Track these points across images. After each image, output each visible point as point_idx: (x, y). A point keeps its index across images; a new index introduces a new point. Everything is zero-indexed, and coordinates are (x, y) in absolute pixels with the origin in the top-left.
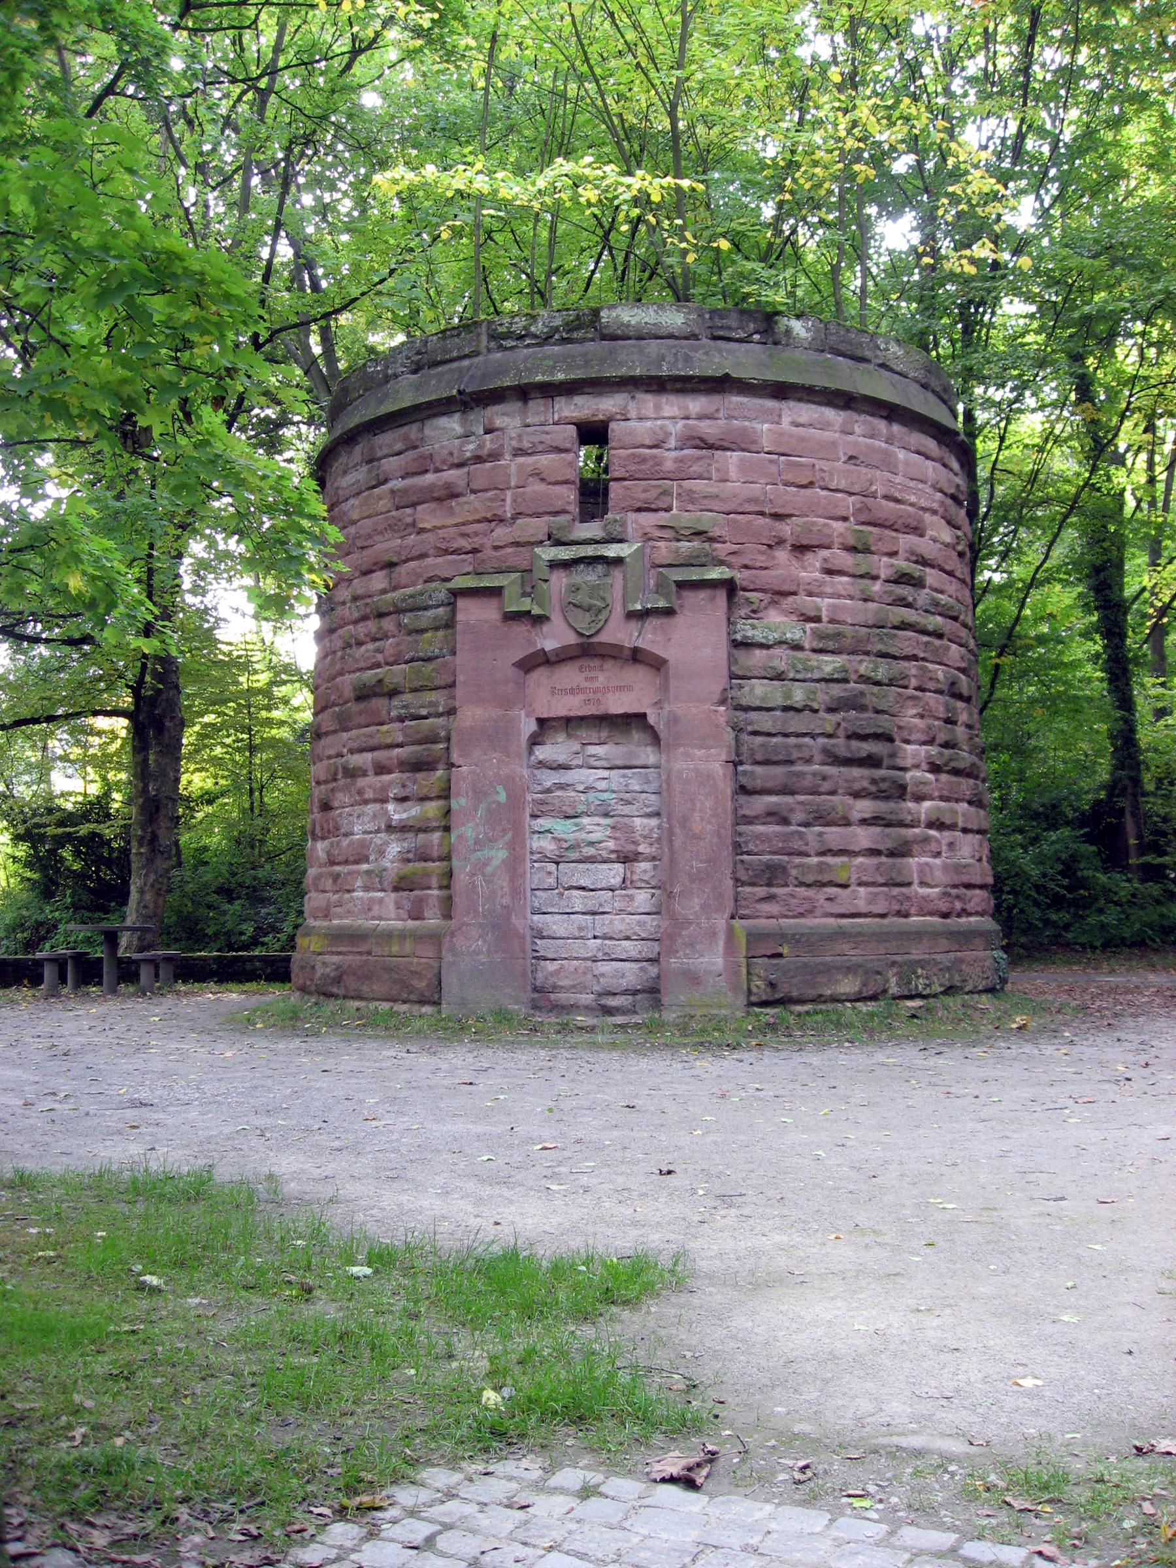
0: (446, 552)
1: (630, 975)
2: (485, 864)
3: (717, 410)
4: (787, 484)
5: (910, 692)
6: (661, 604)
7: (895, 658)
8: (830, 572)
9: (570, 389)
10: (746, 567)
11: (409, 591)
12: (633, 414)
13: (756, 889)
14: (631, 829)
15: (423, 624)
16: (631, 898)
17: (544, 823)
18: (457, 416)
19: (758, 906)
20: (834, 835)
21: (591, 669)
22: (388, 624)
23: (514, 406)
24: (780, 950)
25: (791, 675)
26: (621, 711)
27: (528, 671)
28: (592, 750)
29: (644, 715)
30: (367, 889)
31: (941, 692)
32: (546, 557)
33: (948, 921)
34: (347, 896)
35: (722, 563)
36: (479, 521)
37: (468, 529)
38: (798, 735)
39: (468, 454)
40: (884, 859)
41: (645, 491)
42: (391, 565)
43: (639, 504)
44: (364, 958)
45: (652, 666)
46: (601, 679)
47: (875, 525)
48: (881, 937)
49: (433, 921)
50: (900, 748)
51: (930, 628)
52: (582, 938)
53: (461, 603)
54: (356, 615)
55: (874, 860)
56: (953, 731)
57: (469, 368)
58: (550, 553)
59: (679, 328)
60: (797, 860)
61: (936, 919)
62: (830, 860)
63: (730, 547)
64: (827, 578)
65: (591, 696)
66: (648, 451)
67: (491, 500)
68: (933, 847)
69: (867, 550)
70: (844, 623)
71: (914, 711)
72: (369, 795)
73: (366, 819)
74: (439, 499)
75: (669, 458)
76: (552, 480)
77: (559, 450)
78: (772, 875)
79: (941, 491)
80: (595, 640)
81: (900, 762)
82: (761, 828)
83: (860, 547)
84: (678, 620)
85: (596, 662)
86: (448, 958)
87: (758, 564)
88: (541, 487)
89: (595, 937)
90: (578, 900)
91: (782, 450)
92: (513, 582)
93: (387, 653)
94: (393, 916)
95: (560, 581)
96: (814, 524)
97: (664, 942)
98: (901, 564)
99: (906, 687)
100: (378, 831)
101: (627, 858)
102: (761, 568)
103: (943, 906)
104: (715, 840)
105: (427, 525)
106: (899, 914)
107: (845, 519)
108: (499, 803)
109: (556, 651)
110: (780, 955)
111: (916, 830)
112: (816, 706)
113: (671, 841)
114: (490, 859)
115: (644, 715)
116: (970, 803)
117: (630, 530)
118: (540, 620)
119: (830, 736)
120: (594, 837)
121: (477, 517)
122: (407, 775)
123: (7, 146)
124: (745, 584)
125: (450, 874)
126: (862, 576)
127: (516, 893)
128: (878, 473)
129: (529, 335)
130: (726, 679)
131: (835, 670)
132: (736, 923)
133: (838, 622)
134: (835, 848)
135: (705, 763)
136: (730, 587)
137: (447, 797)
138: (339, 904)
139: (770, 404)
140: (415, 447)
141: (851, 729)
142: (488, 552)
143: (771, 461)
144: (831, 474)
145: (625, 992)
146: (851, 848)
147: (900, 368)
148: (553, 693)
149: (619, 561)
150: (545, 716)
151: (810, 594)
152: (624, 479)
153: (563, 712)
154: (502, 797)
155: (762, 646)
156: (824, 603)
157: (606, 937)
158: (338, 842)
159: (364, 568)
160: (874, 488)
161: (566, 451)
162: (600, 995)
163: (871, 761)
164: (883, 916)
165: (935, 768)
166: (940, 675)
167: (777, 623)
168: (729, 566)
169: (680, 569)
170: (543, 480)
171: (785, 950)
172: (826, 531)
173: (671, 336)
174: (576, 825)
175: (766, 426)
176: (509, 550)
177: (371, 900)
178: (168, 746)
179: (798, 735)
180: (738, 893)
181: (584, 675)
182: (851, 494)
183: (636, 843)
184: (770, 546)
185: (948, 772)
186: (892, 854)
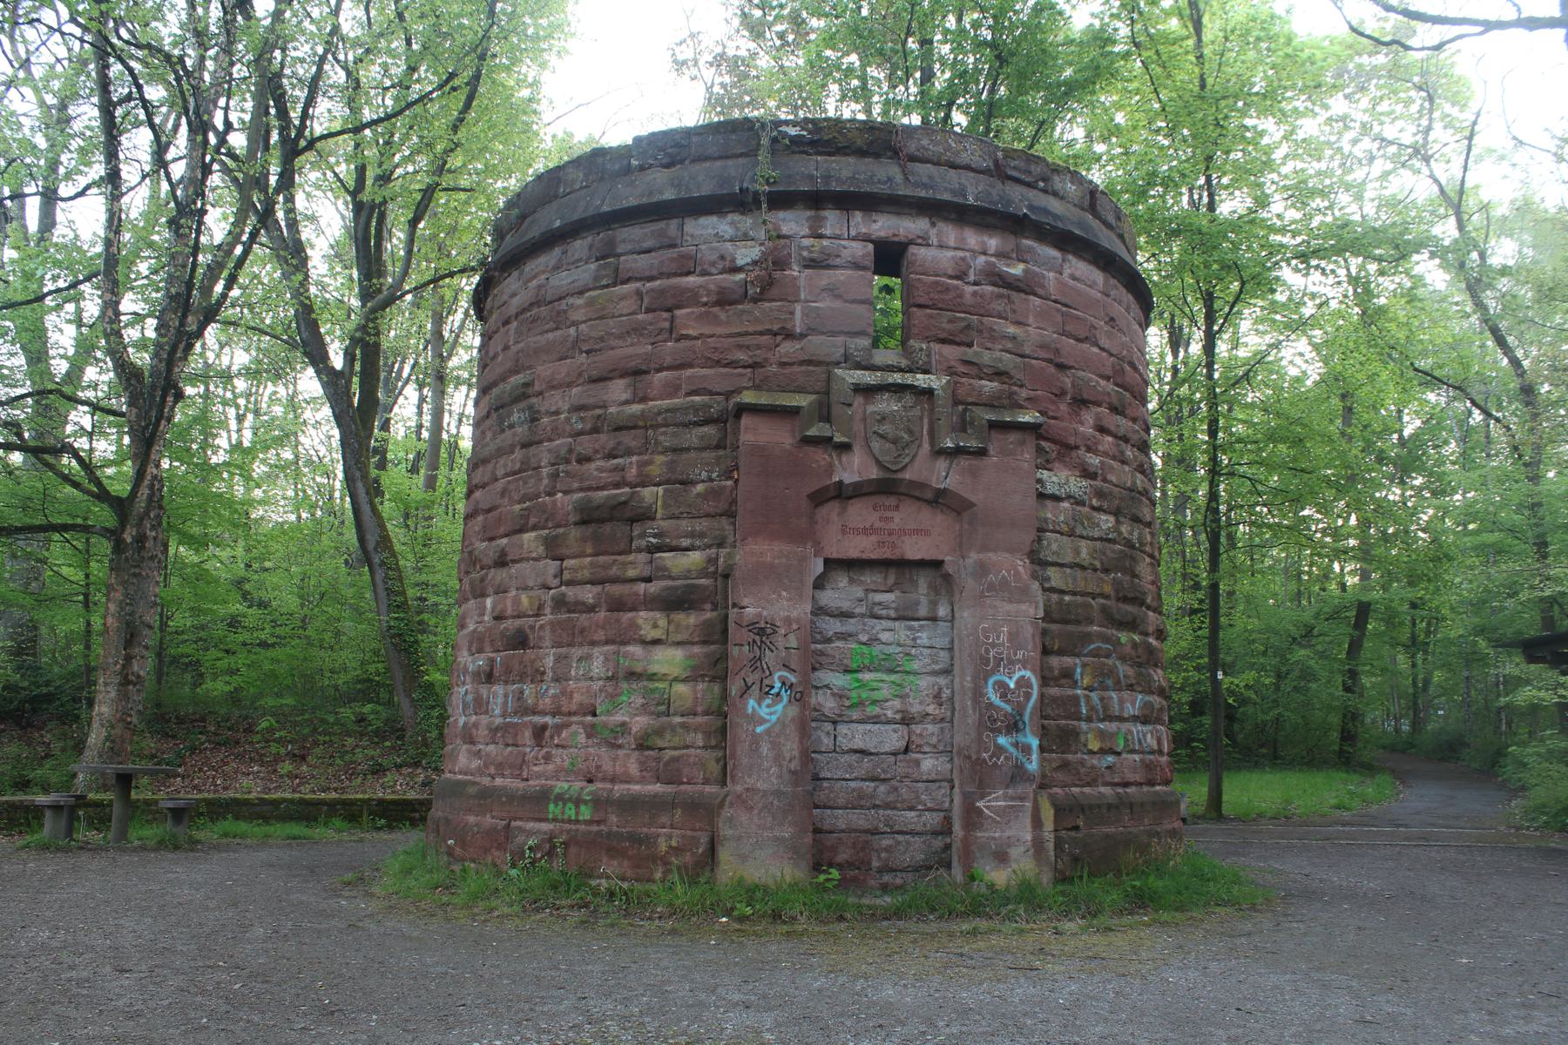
0: (718, 363)
12: (934, 240)
16: (917, 763)
21: (888, 508)
26: (918, 557)
36: (761, 333)
41: (950, 321)
42: (637, 373)
46: (897, 520)
76: (850, 297)
80: (899, 476)
84: (987, 461)
85: (892, 501)
91: (1063, 300)
109: (856, 485)
118: (845, 447)
121: (759, 328)
148: (844, 532)
149: (929, 392)
152: (927, 307)
170: (838, 297)
176: (796, 369)
181: (877, 514)
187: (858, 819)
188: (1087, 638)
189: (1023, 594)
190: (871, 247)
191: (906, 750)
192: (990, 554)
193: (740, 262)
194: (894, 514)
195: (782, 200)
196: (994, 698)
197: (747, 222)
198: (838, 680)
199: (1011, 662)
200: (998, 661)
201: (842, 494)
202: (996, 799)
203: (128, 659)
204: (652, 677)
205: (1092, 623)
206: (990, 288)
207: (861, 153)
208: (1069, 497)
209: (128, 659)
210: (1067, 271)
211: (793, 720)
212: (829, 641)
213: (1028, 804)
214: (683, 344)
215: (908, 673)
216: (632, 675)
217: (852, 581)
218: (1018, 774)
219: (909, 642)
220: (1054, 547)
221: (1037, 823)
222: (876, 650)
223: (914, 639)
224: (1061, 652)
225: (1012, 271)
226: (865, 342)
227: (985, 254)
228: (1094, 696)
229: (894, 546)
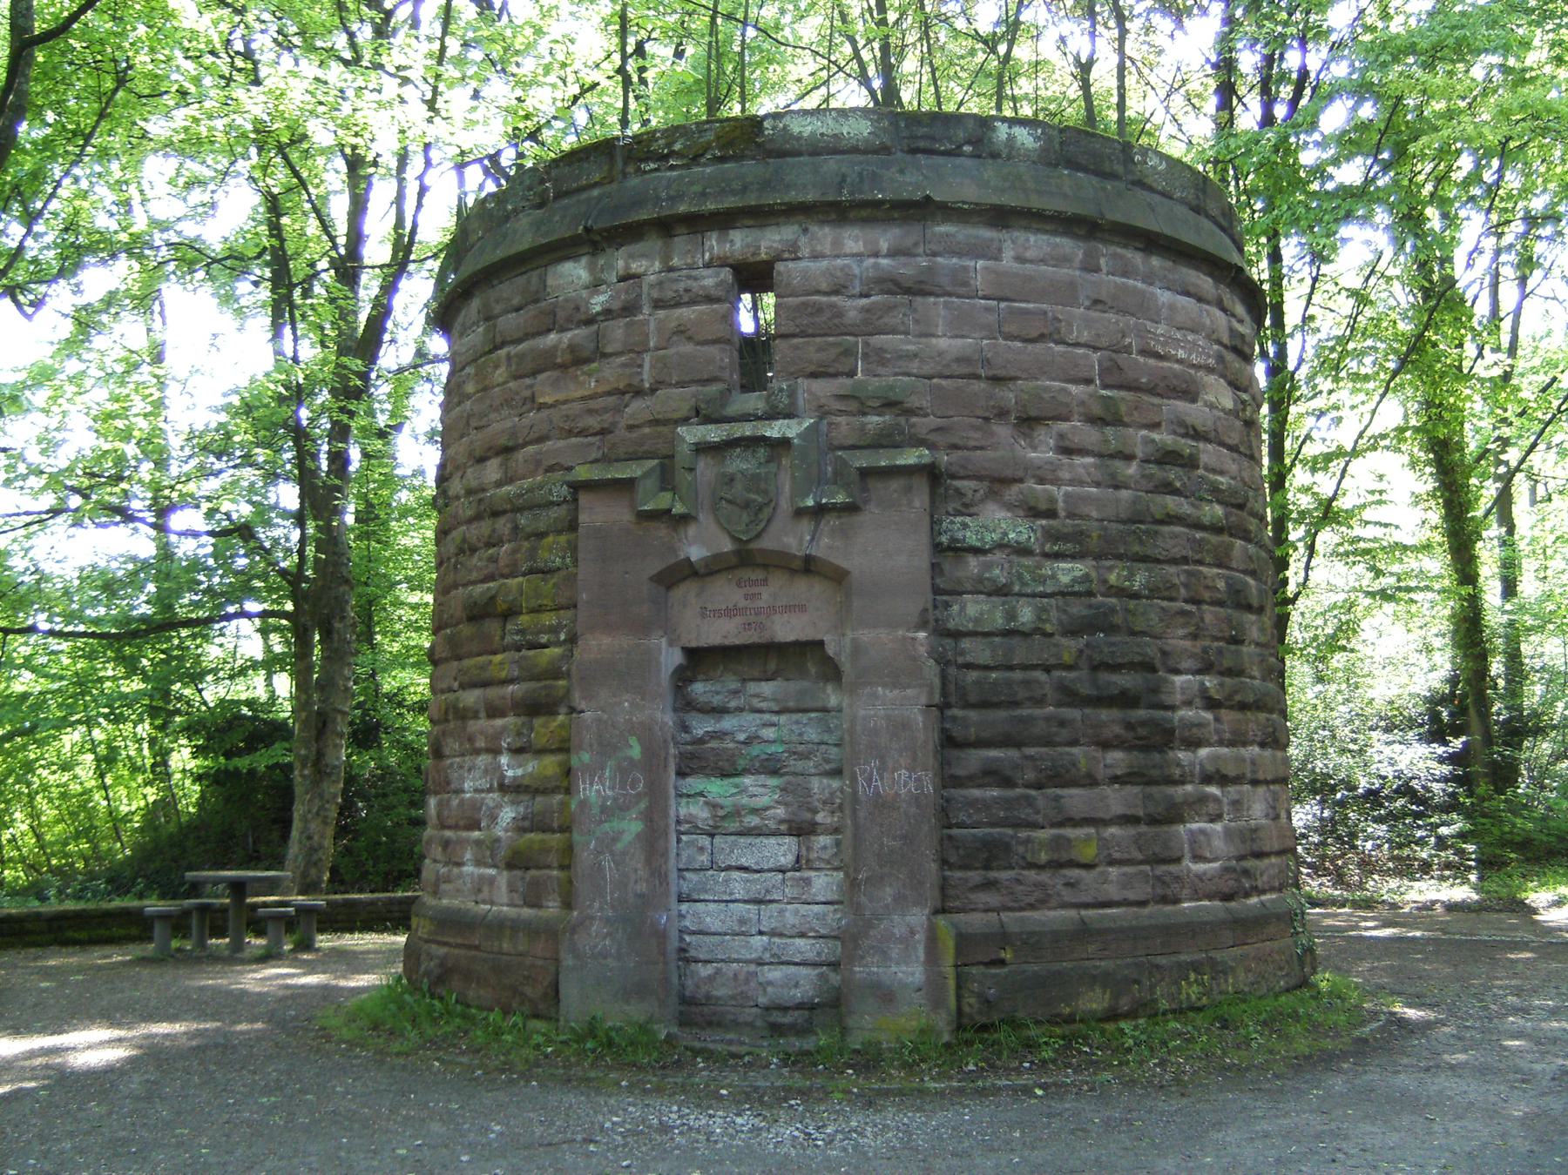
0: (570, 433)
1: (802, 984)
2: (615, 840)
3: (916, 244)
4: (1009, 337)
5: (1180, 605)
6: (840, 498)
7: (1158, 561)
8: (1067, 451)
9: (724, 221)
10: (955, 447)
11: (526, 483)
12: (805, 251)
13: (970, 874)
14: (808, 792)
15: (542, 527)
16: (808, 882)
17: (695, 783)
18: (584, 260)
19: (972, 896)
20: (1075, 799)
21: (755, 583)
22: (503, 525)
23: (653, 243)
24: (1003, 954)
25: (1017, 588)
26: (791, 638)
27: (669, 588)
28: (752, 687)
29: (821, 643)
30: (479, 863)
31: (1220, 603)
32: (690, 439)
33: (1233, 904)
34: (456, 870)
35: (922, 443)
36: (609, 394)
37: (592, 404)
38: (1025, 667)
39: (598, 308)
40: (1143, 828)
41: (820, 349)
42: (507, 450)
43: (812, 368)
44: (473, 953)
45: (831, 579)
46: (765, 596)
47: (1129, 388)
48: (1135, 934)
49: (552, 909)
50: (1166, 681)
51: (1206, 520)
52: (743, 934)
53: (584, 499)
54: (469, 513)
55: (1131, 831)
56: (1238, 653)
57: (599, 199)
58: (691, 434)
59: (866, 140)
60: (1023, 834)
61: (1217, 903)
62: (1069, 832)
63: (932, 421)
64: (1065, 460)
65: (752, 619)
66: (824, 299)
67: (624, 365)
68: (1212, 808)
69: (1118, 422)
70: (1087, 517)
71: (1181, 632)
72: (481, 743)
73: (477, 774)
74: (563, 367)
75: (852, 308)
77: (710, 299)
78: (992, 854)
79: (1219, 343)
80: (753, 546)
81: (1168, 700)
82: (976, 793)
83: (1109, 418)
85: (758, 574)
86: (568, 961)
87: (972, 443)
88: (688, 348)
89: (761, 933)
90: (738, 885)
92: (646, 475)
93: (502, 563)
94: (505, 900)
95: (706, 469)
96: (1047, 389)
97: (851, 940)
98: (1163, 437)
99: (1171, 599)
100: (490, 790)
101: (801, 830)
102: (976, 448)
103: (1228, 885)
104: (913, 810)
105: (548, 400)
106: (1164, 900)
107: (1089, 381)
108: (631, 759)
109: (707, 561)
110: (1002, 962)
111: (1189, 788)
112: (1048, 628)
113: (854, 811)
114: (621, 833)
115: (821, 643)
116: (1263, 745)
117: (801, 402)
118: (685, 519)
119: (1069, 668)
122: (523, 719)
123: (341, 7)
124: (954, 469)
125: (569, 849)
126: (1112, 456)
127: (658, 875)
128: (1133, 320)
129: (672, 154)
130: (930, 596)
131: (1074, 580)
132: (941, 921)
133: (1081, 517)
134: (1077, 817)
135: (890, 708)
136: (933, 474)
137: (567, 751)
138: (448, 880)
139: (987, 233)
140: (536, 301)
141: (1097, 658)
142: (621, 433)
143: (987, 309)
144: (1070, 325)
145: (799, 1006)
146: (1101, 815)
147: (1161, 185)
148: (703, 616)
149: (785, 443)
150: (694, 644)
151: (1041, 481)
152: (794, 336)
154: (636, 752)
155: (977, 551)
156: (1059, 493)
157: (773, 933)
158: (449, 800)
159: (478, 454)
160: (1128, 340)
161: (718, 300)
162: (767, 1009)
163: (1126, 700)
164: (1142, 904)
165: (1211, 704)
166: (1221, 585)
167: (997, 522)
168: (932, 446)
169: (866, 452)
170: (690, 339)
171: (1007, 955)
172: (1061, 398)
173: (855, 150)
174: (736, 786)
175: (980, 263)
177: (482, 877)
178: (337, 650)
179: (1025, 667)
180: (944, 879)
182: (1096, 349)
183: (815, 812)
184: (986, 419)
185: (1231, 708)
186: (1153, 821)
194: (762, 589)
201: (685, 572)
211: (638, 835)
214: (545, 413)
215: (795, 774)
219: (794, 738)
222: (755, 750)
223: (800, 735)
229: (761, 627)
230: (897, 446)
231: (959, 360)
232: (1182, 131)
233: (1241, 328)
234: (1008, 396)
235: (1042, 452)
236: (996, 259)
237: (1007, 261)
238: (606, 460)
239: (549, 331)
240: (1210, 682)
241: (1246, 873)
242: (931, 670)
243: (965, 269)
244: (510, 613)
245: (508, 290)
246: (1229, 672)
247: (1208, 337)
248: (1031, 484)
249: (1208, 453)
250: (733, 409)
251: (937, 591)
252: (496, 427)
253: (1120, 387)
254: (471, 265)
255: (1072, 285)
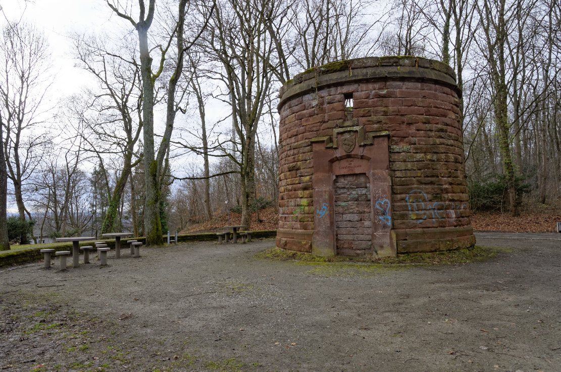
16: (363, 223)
24: (406, 238)
25: (407, 160)
32: (336, 131)
35: (386, 130)
51: (449, 144)
53: (314, 145)
69: (429, 123)
76: (337, 110)
80: (350, 153)
85: (351, 159)
98: (440, 126)
105: (305, 124)
107: (423, 114)
120: (353, 207)
130: (388, 162)
136: (388, 136)
143: (399, 100)
149: (356, 131)
153: (342, 173)
165: (451, 184)
167: (403, 146)
168: (388, 130)
170: (335, 110)
175: (398, 90)
187: (350, 237)
188: (411, 189)
189: (385, 180)
190: (343, 95)
191: (361, 220)
192: (376, 171)
193: (313, 105)
195: (321, 88)
196: (378, 207)
197: (314, 95)
198: (343, 204)
199: (382, 197)
200: (379, 197)
202: (380, 232)
203: (248, 200)
204: (301, 205)
205: (413, 184)
206: (376, 99)
207: (340, 71)
208: (404, 152)
209: (248, 200)
210: (404, 87)
211: (327, 215)
212: (340, 194)
213: (388, 234)
216: (298, 205)
217: (344, 180)
218: (385, 226)
220: (398, 166)
221: (391, 239)
224: (401, 193)
225: (383, 93)
226: (341, 121)
227: (375, 89)
228: (415, 204)
230: (380, 131)
231: (393, 112)
232: (432, 48)
233: (456, 100)
234: (405, 119)
235: (412, 129)
236: (401, 89)
237: (404, 89)
238: (318, 136)
239: (304, 110)
240: (450, 179)
241: (460, 221)
242: (389, 178)
243: (394, 91)
244: (298, 169)
245: (295, 102)
246: (455, 177)
247: (449, 102)
248: (410, 138)
249: (449, 129)
250: (345, 125)
251: (390, 161)
252: (293, 130)
253: (429, 115)
254: (284, 97)
255: (418, 93)
